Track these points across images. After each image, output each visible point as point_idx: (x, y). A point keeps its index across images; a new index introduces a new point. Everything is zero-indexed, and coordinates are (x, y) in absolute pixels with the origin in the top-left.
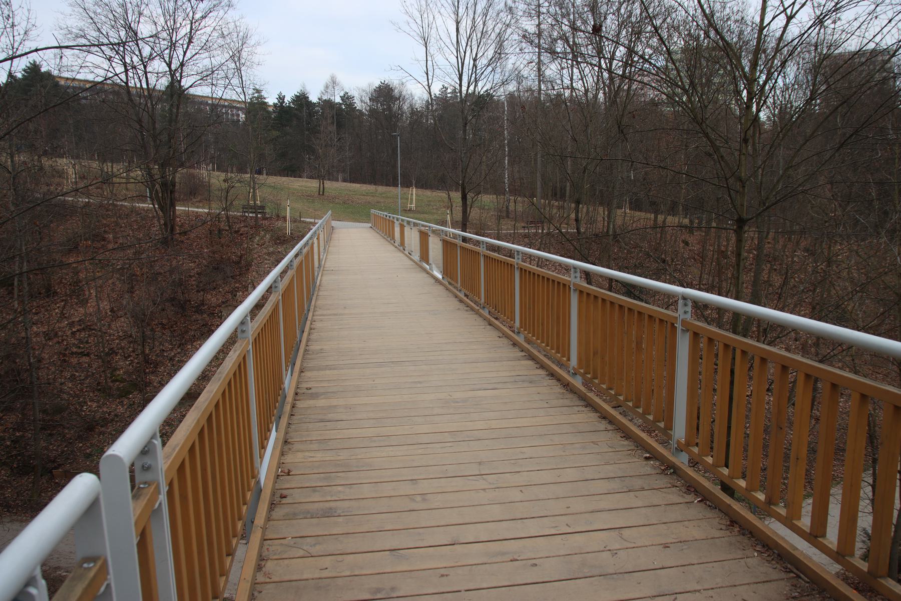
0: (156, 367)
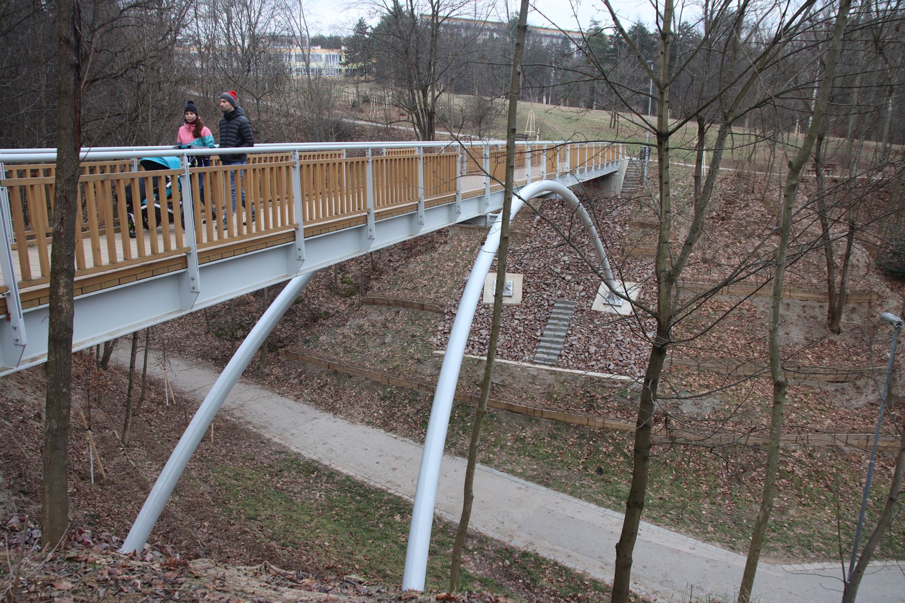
0: (380, 275)
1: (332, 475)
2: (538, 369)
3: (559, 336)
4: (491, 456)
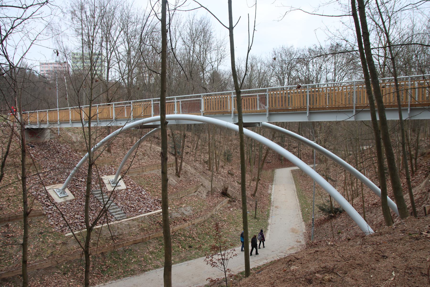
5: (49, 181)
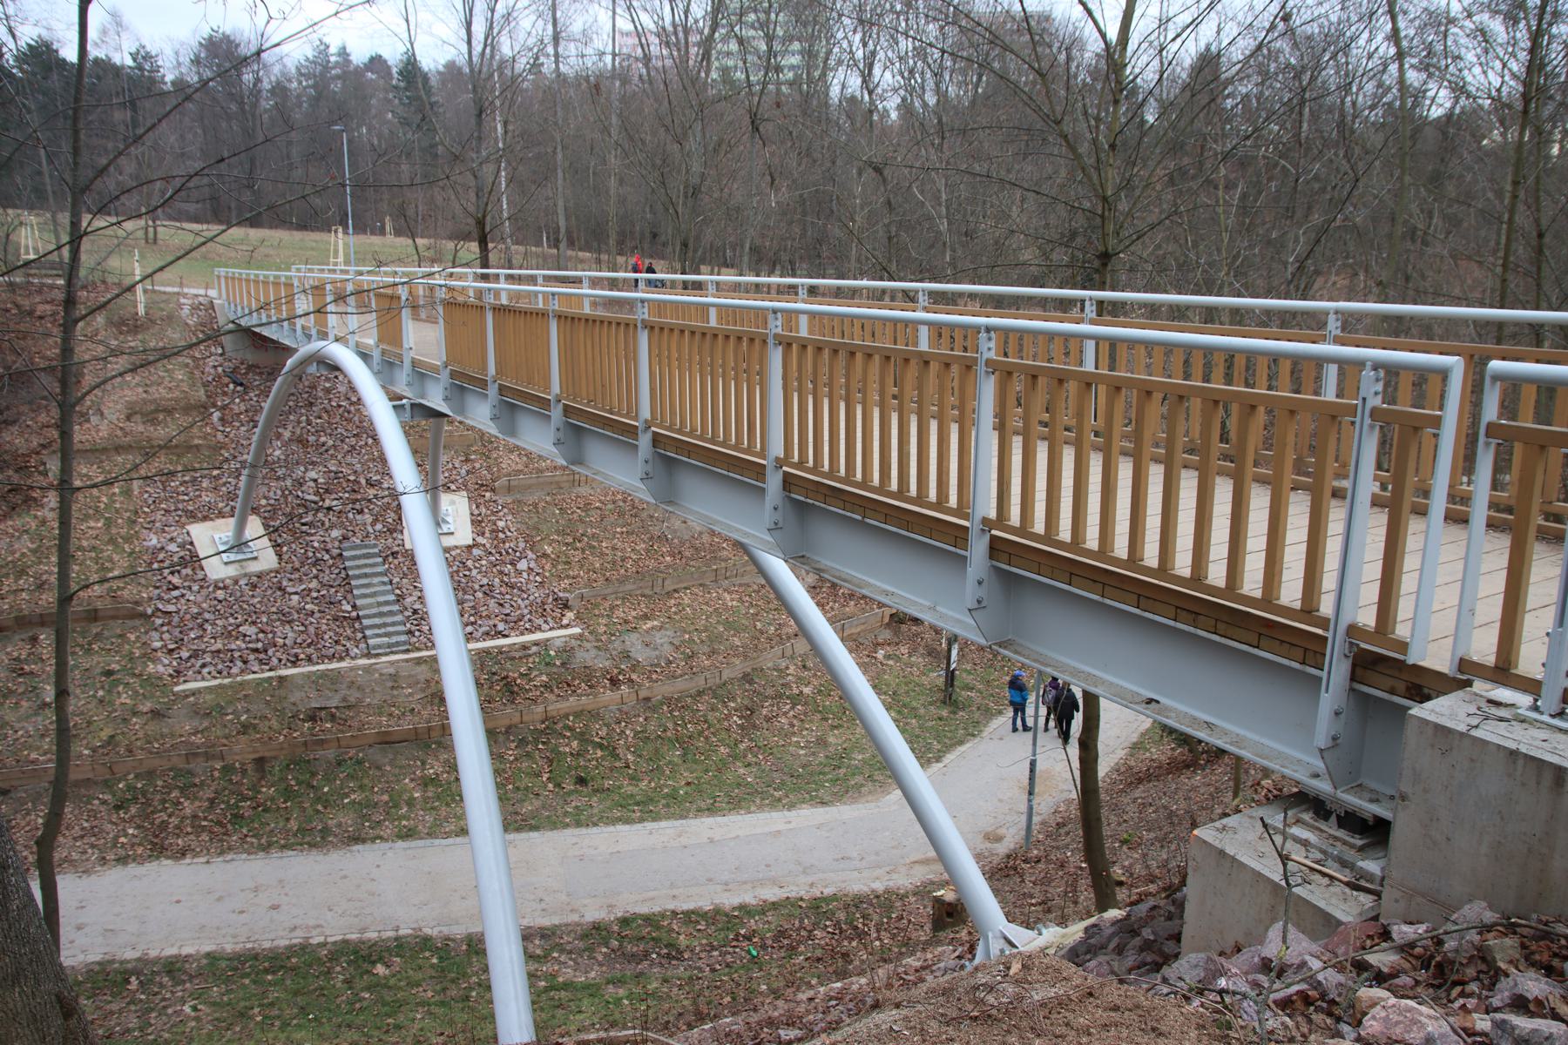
1: (173, 967)
2: (392, 663)
3: (387, 603)
4: (404, 822)
5: (221, 505)
